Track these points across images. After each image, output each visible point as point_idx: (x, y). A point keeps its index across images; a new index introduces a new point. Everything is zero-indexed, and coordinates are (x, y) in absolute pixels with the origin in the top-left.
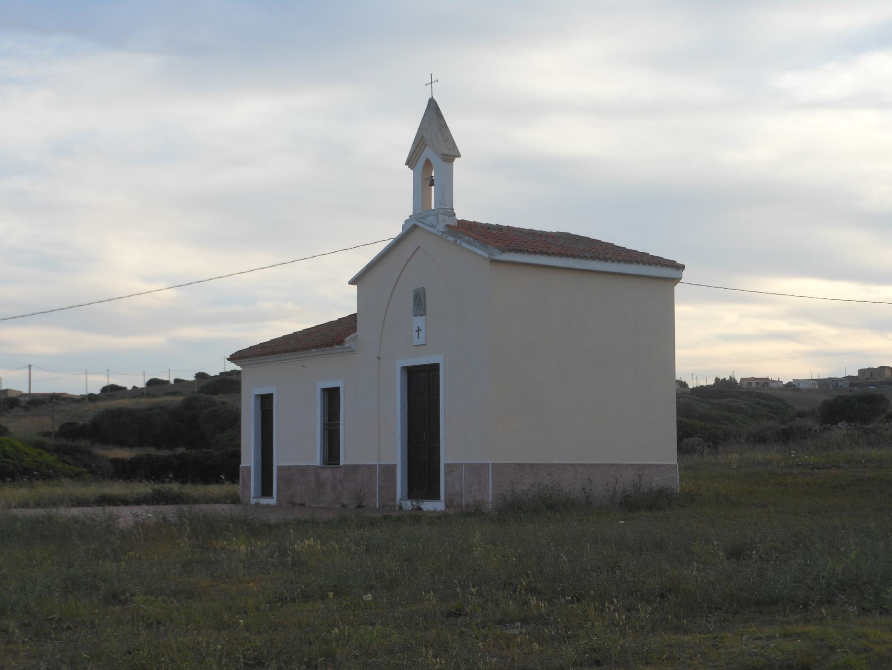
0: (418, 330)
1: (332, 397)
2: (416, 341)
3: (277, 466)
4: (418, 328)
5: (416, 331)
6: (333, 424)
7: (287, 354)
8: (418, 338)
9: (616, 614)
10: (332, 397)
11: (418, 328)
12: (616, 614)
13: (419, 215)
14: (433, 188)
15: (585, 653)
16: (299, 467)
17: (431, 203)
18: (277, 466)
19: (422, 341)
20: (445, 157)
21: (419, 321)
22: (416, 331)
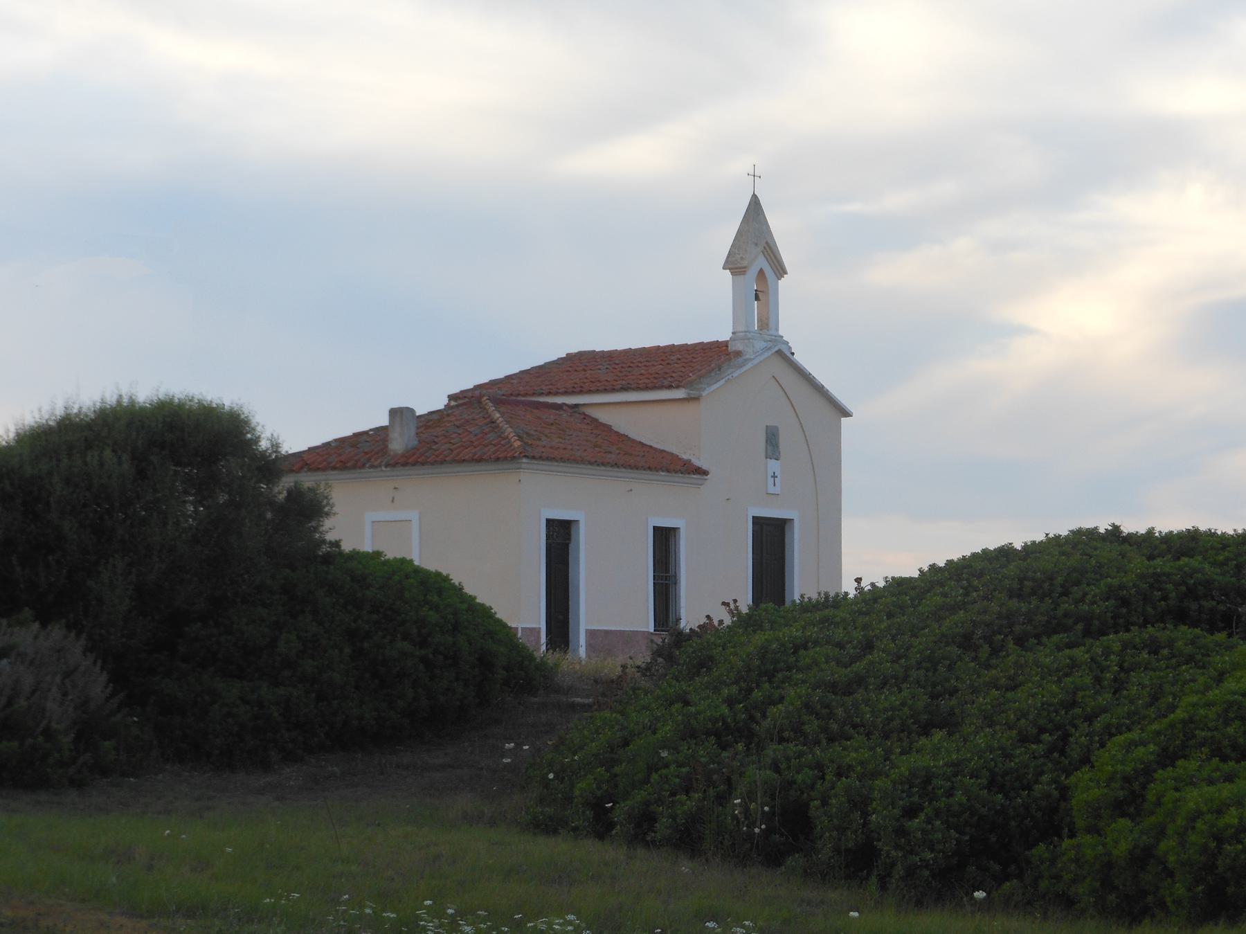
0: (774, 476)
1: (664, 539)
2: (771, 490)
3: (587, 630)
4: (774, 473)
5: (777, 477)
6: (662, 580)
7: (407, 468)
8: (774, 485)
9: (479, 912)
10: (664, 539)
11: (774, 473)
12: (479, 912)
13: (434, 438)
14: (755, 288)
15: (817, 653)
16: (622, 633)
17: (754, 319)
18: (587, 630)
19: (777, 490)
20: (766, 247)
21: (773, 465)
22: (777, 477)
